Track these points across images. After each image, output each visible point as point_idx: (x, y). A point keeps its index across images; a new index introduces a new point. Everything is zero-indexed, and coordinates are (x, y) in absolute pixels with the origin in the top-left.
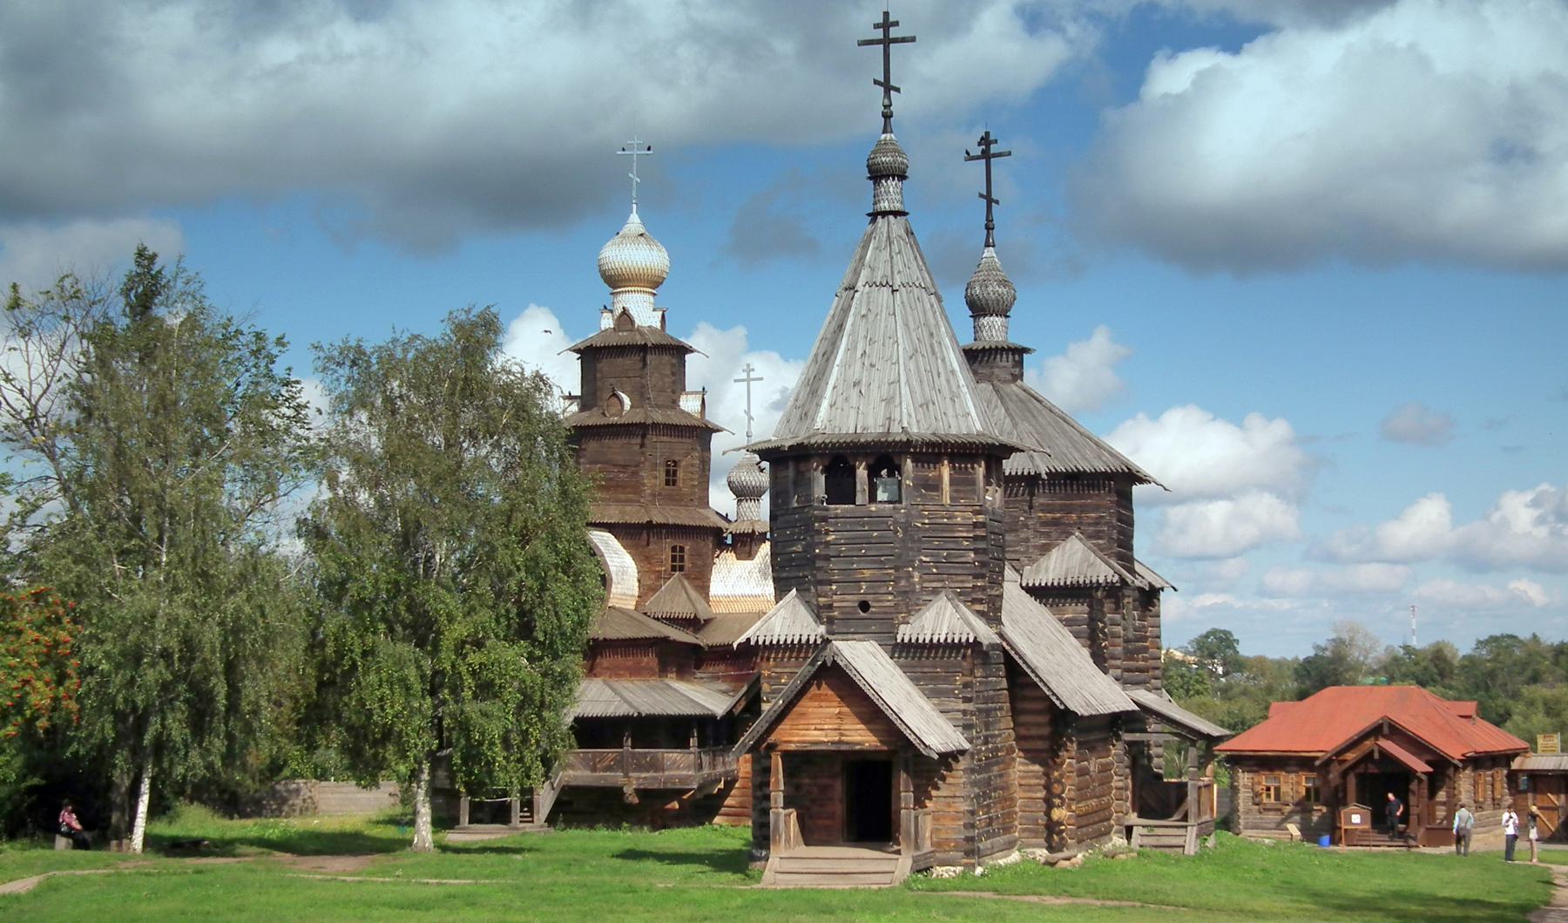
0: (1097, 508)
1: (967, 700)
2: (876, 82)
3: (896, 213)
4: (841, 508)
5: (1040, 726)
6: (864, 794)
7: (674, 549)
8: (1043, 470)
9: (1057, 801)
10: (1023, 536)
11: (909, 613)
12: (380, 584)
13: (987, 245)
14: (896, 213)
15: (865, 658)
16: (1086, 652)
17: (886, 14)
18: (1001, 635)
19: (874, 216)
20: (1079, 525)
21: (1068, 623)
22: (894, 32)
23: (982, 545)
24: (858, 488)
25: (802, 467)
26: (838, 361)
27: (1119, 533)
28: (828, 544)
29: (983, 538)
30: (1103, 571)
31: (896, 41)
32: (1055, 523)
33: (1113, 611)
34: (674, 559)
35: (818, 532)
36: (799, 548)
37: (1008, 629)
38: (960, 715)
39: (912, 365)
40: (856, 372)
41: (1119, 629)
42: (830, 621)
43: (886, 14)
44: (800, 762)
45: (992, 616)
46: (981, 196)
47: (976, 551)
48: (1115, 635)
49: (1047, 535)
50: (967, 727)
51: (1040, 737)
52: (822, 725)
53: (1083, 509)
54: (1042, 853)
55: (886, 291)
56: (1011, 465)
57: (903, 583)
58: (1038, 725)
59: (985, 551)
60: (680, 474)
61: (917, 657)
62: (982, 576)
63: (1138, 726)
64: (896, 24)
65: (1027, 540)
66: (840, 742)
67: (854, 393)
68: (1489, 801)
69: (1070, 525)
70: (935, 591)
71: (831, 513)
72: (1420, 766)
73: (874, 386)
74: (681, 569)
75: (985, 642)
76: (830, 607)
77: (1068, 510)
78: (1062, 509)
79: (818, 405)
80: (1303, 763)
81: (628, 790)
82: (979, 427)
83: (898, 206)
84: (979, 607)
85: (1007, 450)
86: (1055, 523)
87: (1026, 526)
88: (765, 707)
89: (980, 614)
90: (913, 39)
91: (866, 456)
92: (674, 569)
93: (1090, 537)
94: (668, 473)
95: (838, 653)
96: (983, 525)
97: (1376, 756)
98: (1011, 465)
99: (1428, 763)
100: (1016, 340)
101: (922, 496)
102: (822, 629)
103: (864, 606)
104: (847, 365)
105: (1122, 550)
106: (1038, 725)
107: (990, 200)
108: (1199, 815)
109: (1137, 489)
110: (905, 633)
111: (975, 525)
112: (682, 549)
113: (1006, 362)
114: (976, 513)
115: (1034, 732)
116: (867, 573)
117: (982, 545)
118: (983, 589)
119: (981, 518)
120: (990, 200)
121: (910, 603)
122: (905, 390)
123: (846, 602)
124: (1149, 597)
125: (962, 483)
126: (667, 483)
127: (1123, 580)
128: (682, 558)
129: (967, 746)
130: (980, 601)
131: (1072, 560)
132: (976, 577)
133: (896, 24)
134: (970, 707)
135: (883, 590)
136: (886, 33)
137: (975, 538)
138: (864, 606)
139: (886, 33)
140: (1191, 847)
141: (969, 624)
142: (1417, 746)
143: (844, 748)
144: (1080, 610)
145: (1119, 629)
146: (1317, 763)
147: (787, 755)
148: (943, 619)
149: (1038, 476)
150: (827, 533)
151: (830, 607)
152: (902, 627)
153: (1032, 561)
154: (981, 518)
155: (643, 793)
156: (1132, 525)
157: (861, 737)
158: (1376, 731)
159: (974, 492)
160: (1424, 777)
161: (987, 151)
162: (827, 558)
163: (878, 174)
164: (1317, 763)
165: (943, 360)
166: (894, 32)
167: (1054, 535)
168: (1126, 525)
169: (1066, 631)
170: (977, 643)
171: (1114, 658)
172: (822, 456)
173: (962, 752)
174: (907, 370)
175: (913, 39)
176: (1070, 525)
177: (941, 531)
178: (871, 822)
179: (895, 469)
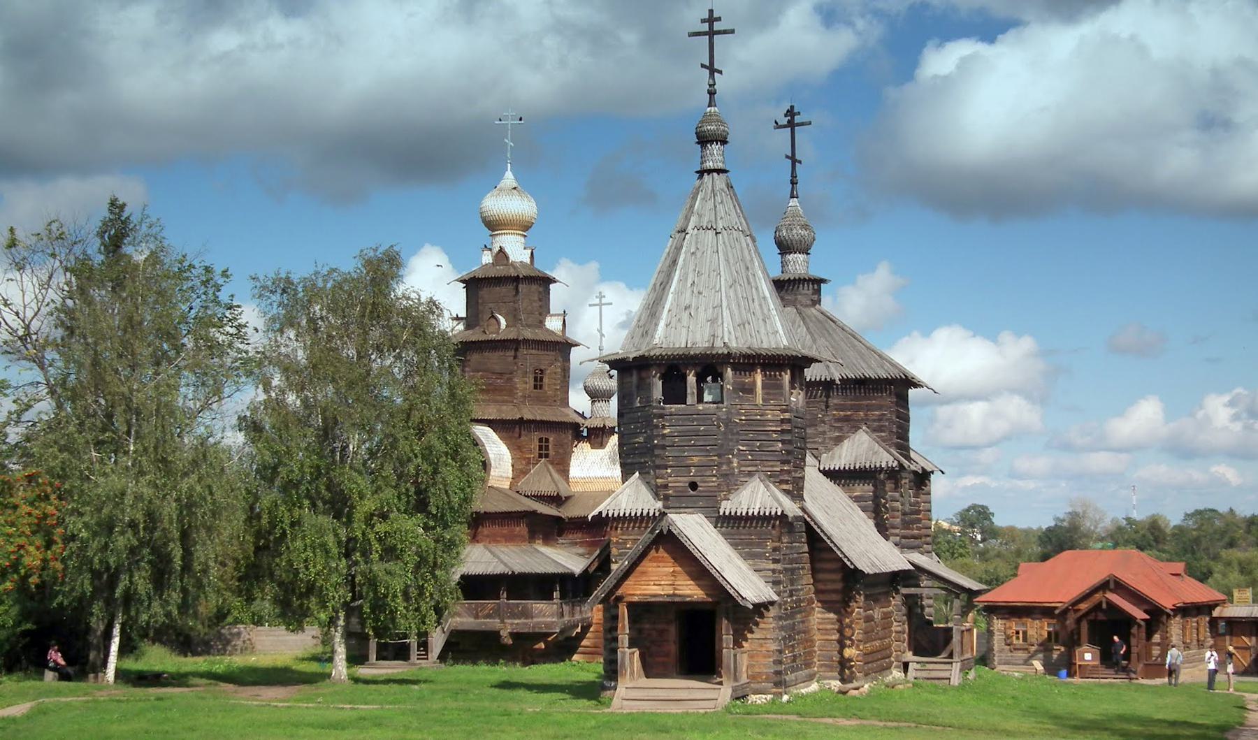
0: (880, 408)
1: (776, 561)
2: (703, 66)
3: (719, 171)
4: (674, 408)
5: (834, 582)
6: (694, 636)
7: (541, 440)
8: (837, 377)
9: (848, 642)
10: (820, 429)
11: (729, 491)
12: (305, 468)
13: (792, 197)
14: (719, 171)
15: (694, 528)
16: (871, 523)
17: (711, 11)
18: (803, 510)
19: (701, 173)
20: (865, 421)
21: (857, 499)
22: (717, 26)
23: (787, 437)
24: (689, 391)
25: (644, 374)
26: (672, 289)
27: (898, 427)
28: (664, 436)
29: (789, 431)
30: (885, 458)
31: (719, 32)
32: (846, 419)
33: (893, 490)
34: (540, 448)
35: (657, 427)
36: (641, 439)
37: (809, 505)
38: (770, 573)
39: (732, 293)
40: (687, 298)
41: (898, 504)
42: (666, 498)
43: (711, 11)
44: (642, 611)
45: (796, 493)
46: (787, 157)
47: (783, 442)
48: (895, 510)
49: (840, 429)
50: (776, 583)
51: (835, 591)
52: (659, 582)
53: (869, 408)
54: (836, 684)
55: (711, 233)
56: (811, 373)
57: (724, 467)
58: (833, 581)
59: (790, 442)
60: (546, 380)
61: (735, 527)
62: (788, 462)
63: (912, 582)
64: (719, 19)
65: (824, 433)
66: (674, 595)
67: (685, 315)
68: (1195, 642)
69: (858, 421)
70: (750, 474)
71: (667, 412)
72: (1139, 614)
73: (701, 309)
74: (547, 456)
75: (790, 515)
76: (666, 487)
77: (857, 409)
78: (852, 408)
79: (657, 325)
80: (1045, 612)
81: (504, 633)
82: (786, 343)
83: (720, 165)
84: (785, 487)
85: (808, 361)
86: (846, 419)
87: (824, 422)
88: (614, 567)
89: (787, 492)
90: (732, 32)
91: (695, 365)
92: (540, 456)
93: (874, 430)
94: (536, 379)
95: (672, 523)
96: (789, 421)
97: (1104, 606)
98: (811, 373)
99: (1146, 612)
100: (815, 273)
101: (740, 397)
102: (659, 505)
103: (694, 486)
104: (679, 293)
105: (900, 440)
106: (833, 581)
107: (794, 161)
108: (962, 653)
109: (912, 392)
110: (727, 507)
111: (783, 421)
112: (547, 440)
113: (807, 290)
114: (783, 411)
115: (830, 587)
116: (696, 460)
117: (787, 437)
118: (789, 472)
119: (787, 415)
120: (794, 161)
121: (730, 483)
122: (726, 313)
123: (679, 482)
124: (922, 479)
125: (772, 387)
126: (535, 387)
127: (901, 465)
128: (547, 448)
129: (776, 598)
130: (787, 482)
131: (860, 449)
132: (783, 462)
133: (719, 19)
134: (778, 566)
135: (708, 473)
136: (711, 26)
137: (783, 431)
138: (694, 486)
139: (711, 26)
140: (956, 680)
141: (778, 500)
142: (1137, 598)
143: (677, 599)
144: (866, 489)
145: (898, 504)
146: (1057, 612)
147: (631, 606)
148: (757, 496)
149: (833, 381)
150: (664, 427)
151: (666, 487)
152: (724, 503)
153: (828, 450)
154: (787, 415)
155: (515, 636)
156: (908, 421)
157: (691, 591)
158: (1104, 586)
159: (782, 394)
160: (1142, 623)
161: (792, 121)
162: (664, 447)
163: (704, 140)
164: (1057, 612)
165: (757, 288)
166: (717, 26)
167: (846, 429)
168: (903, 421)
169: (855, 506)
170: (784, 516)
171: (894, 527)
172: (659, 365)
173: (772, 603)
174: (728, 297)
175: (732, 32)
176: (858, 421)
177: (755, 426)
178: (699, 659)
179: (718, 376)
